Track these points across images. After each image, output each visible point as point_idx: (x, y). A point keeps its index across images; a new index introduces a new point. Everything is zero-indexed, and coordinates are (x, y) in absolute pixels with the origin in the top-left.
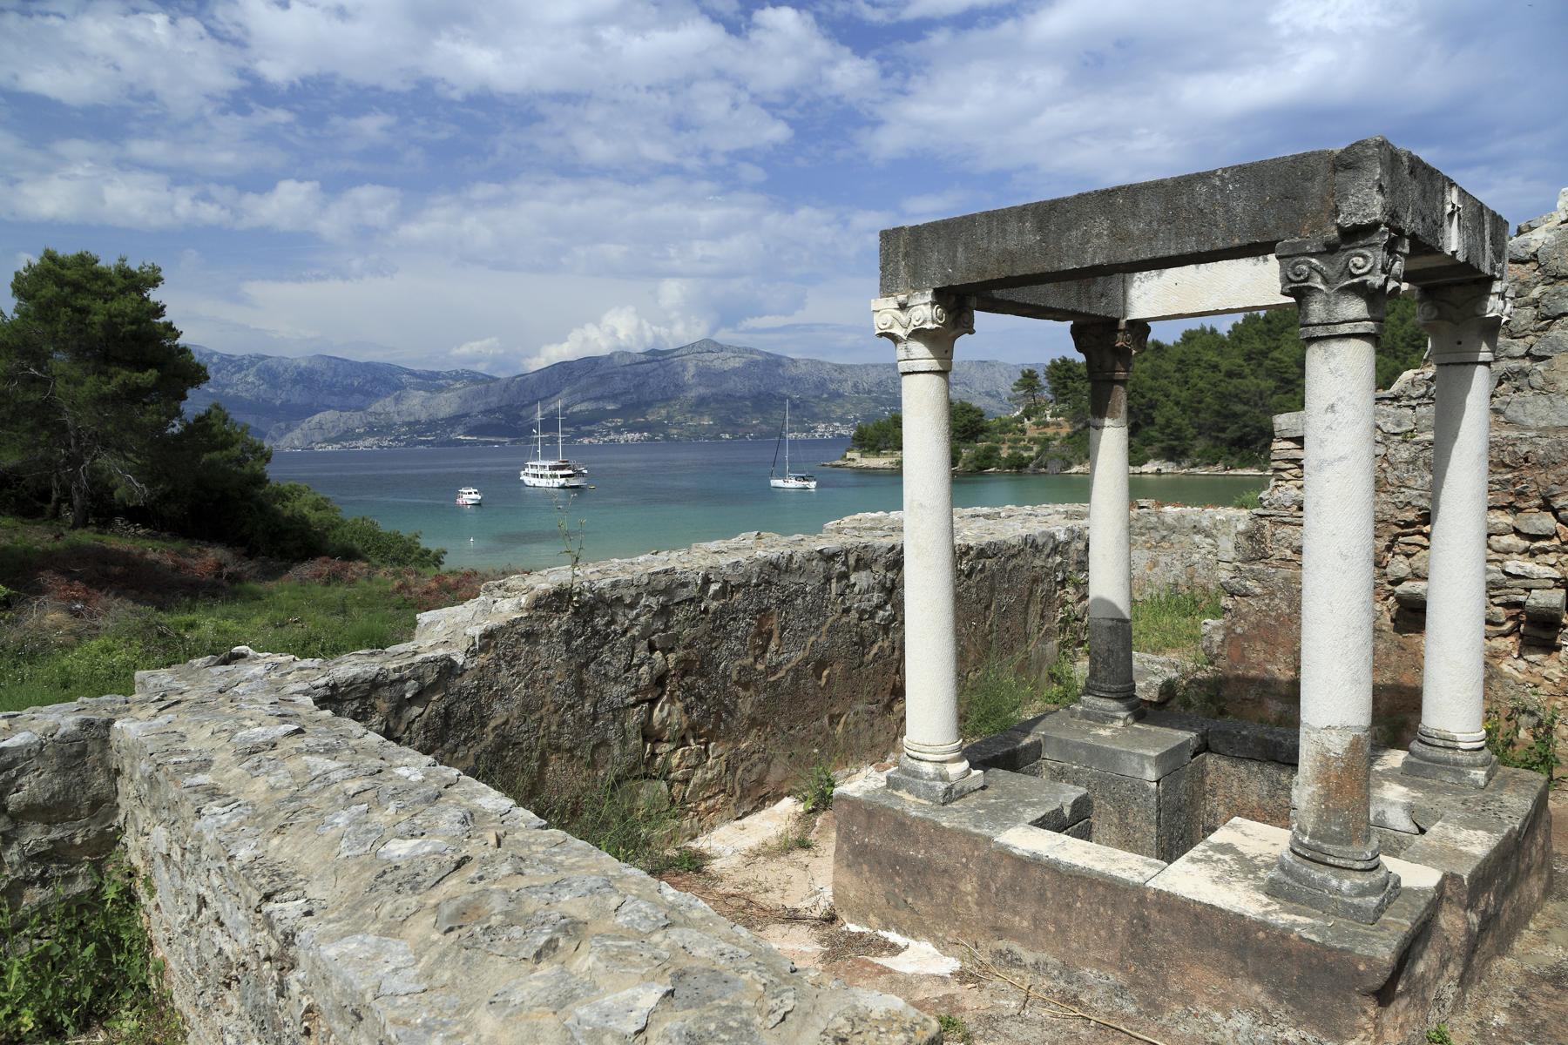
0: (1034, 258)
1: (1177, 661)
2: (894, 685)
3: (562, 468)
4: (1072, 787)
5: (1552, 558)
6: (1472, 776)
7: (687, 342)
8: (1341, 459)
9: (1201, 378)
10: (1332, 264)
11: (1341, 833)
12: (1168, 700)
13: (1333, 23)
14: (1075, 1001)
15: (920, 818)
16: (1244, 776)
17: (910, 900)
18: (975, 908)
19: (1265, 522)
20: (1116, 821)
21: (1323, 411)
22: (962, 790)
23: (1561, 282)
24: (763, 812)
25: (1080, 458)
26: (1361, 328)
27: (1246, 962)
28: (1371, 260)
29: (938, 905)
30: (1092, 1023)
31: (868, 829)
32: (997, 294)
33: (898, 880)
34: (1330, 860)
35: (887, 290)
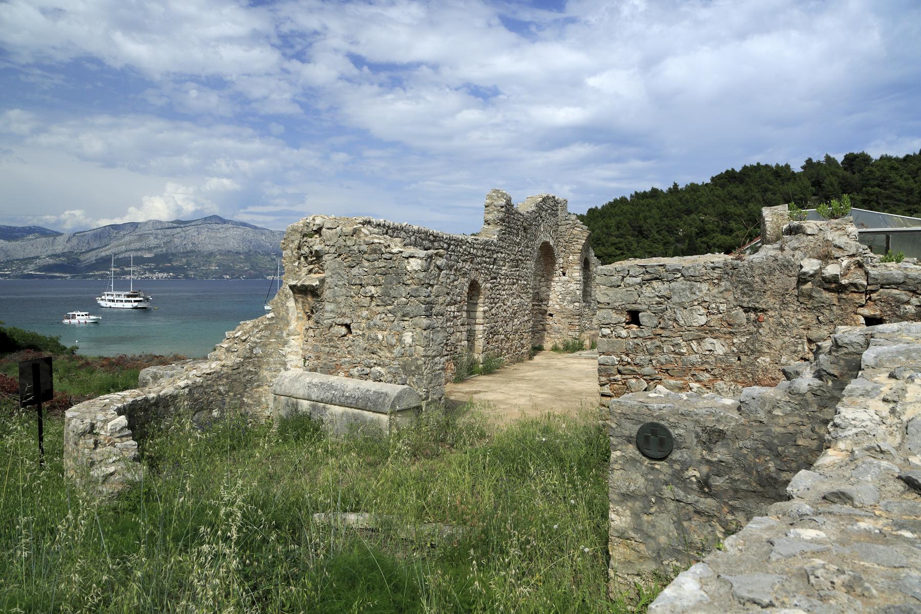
3: (135, 296)
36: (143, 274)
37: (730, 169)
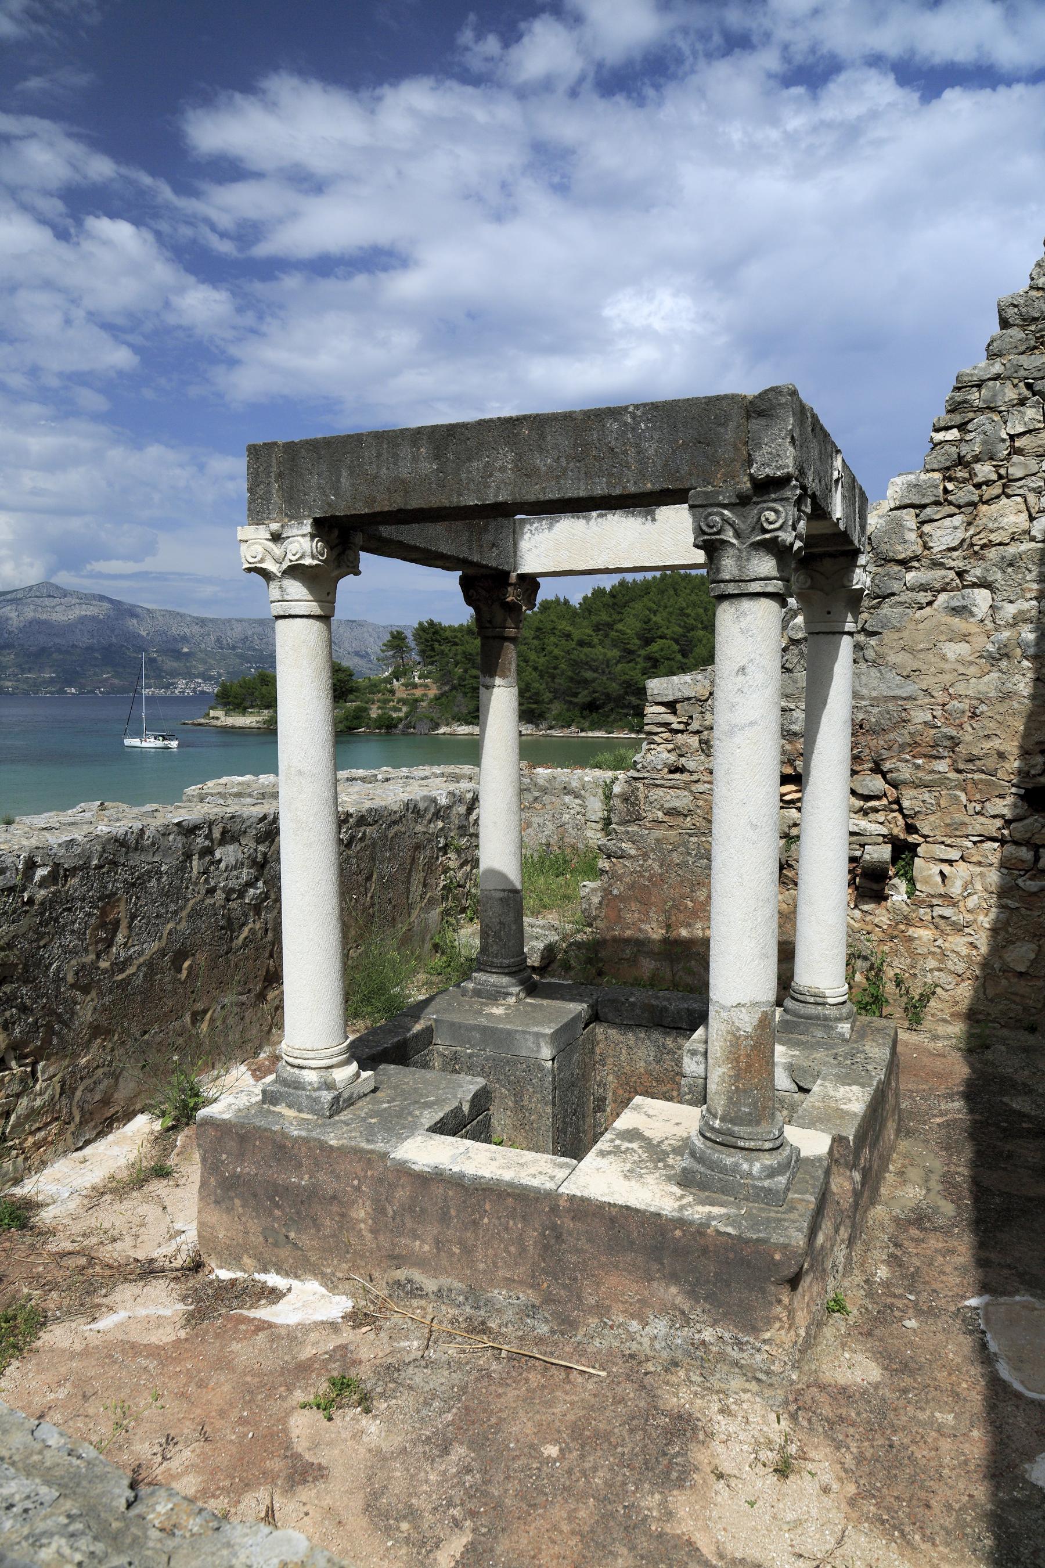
0: (430, 489)
1: (556, 923)
2: (268, 971)
4: (469, 1078)
5: (881, 817)
6: (839, 1030)
7: (18, 584)
8: (752, 724)
9: (557, 645)
10: (743, 517)
11: (750, 1114)
12: (548, 965)
13: (658, 325)
14: (483, 1329)
15: (303, 1138)
16: (631, 1043)
17: (292, 1235)
18: (368, 1236)
19: (639, 784)
20: (511, 1104)
21: (734, 673)
22: (350, 1098)
23: (889, 565)
24: (111, 1137)
25: (446, 719)
26: (771, 587)
27: (662, 1264)
28: (783, 515)
29: (326, 1237)
30: (504, 1354)
31: (241, 1156)
32: (386, 531)
33: (277, 1213)
34: (741, 1144)
35: (256, 517)
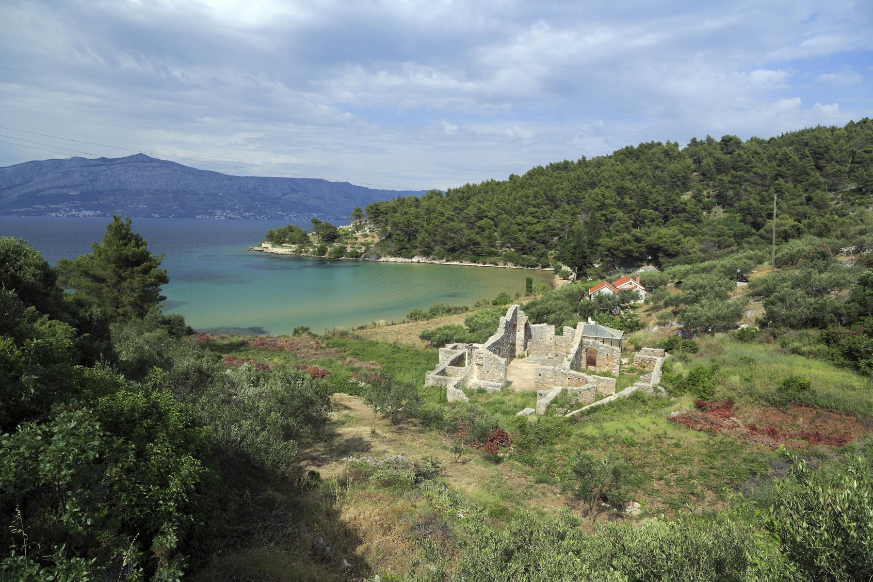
36: (69, 212)
37: (629, 146)
